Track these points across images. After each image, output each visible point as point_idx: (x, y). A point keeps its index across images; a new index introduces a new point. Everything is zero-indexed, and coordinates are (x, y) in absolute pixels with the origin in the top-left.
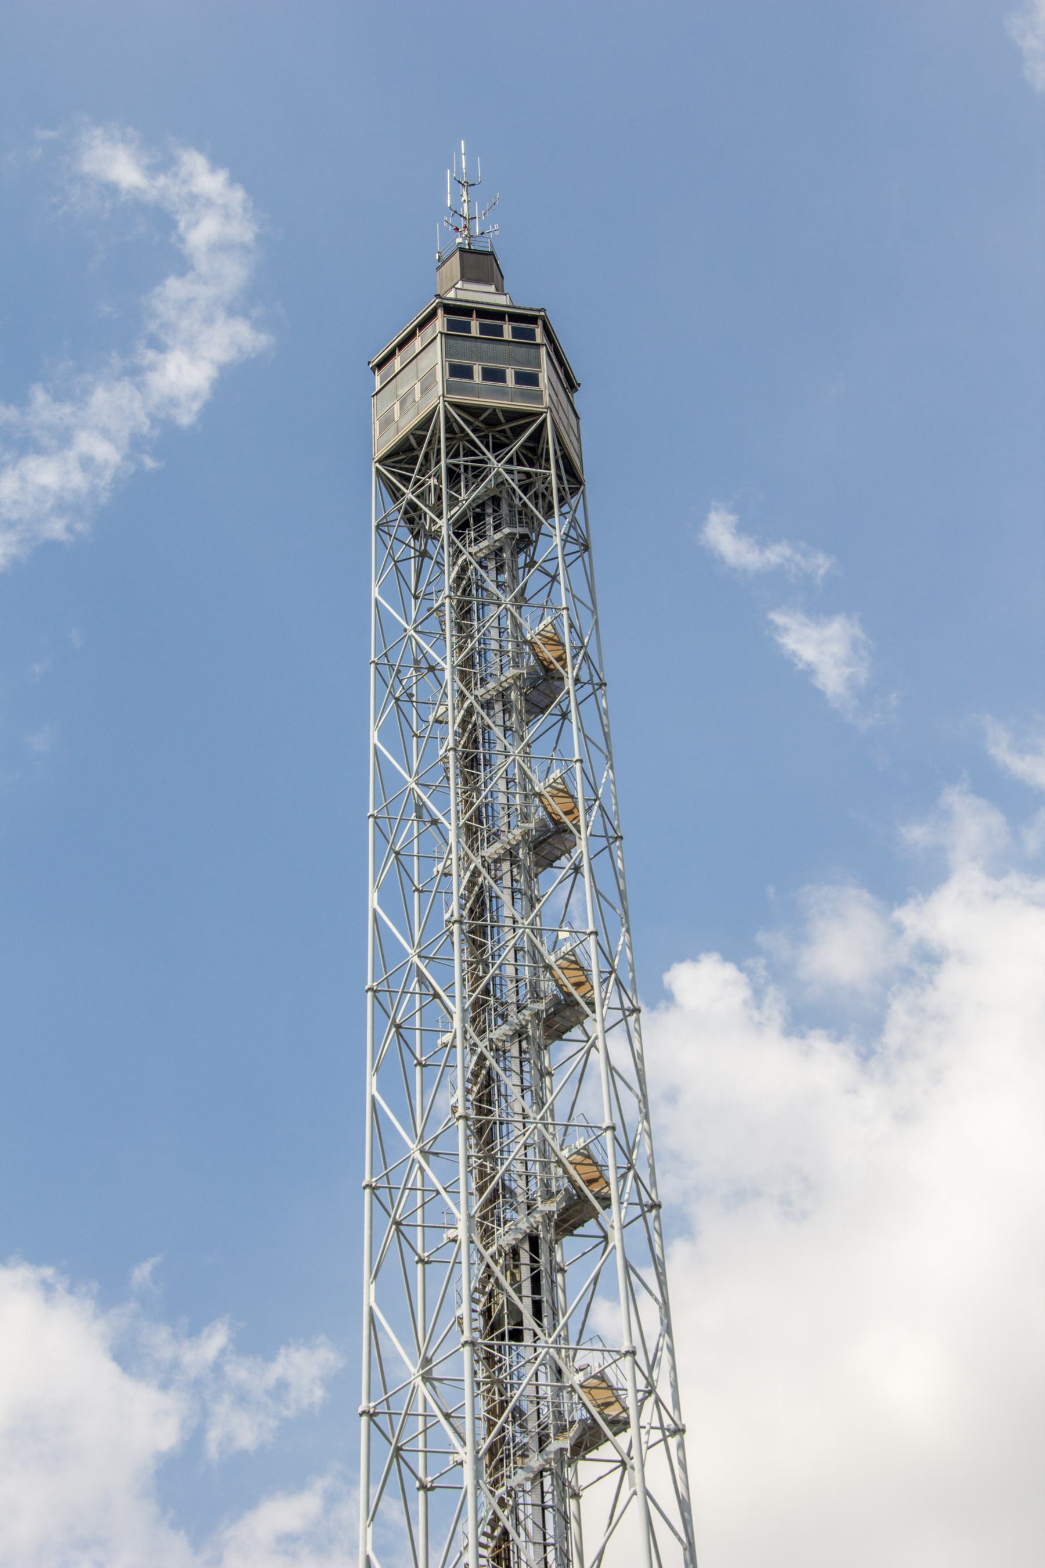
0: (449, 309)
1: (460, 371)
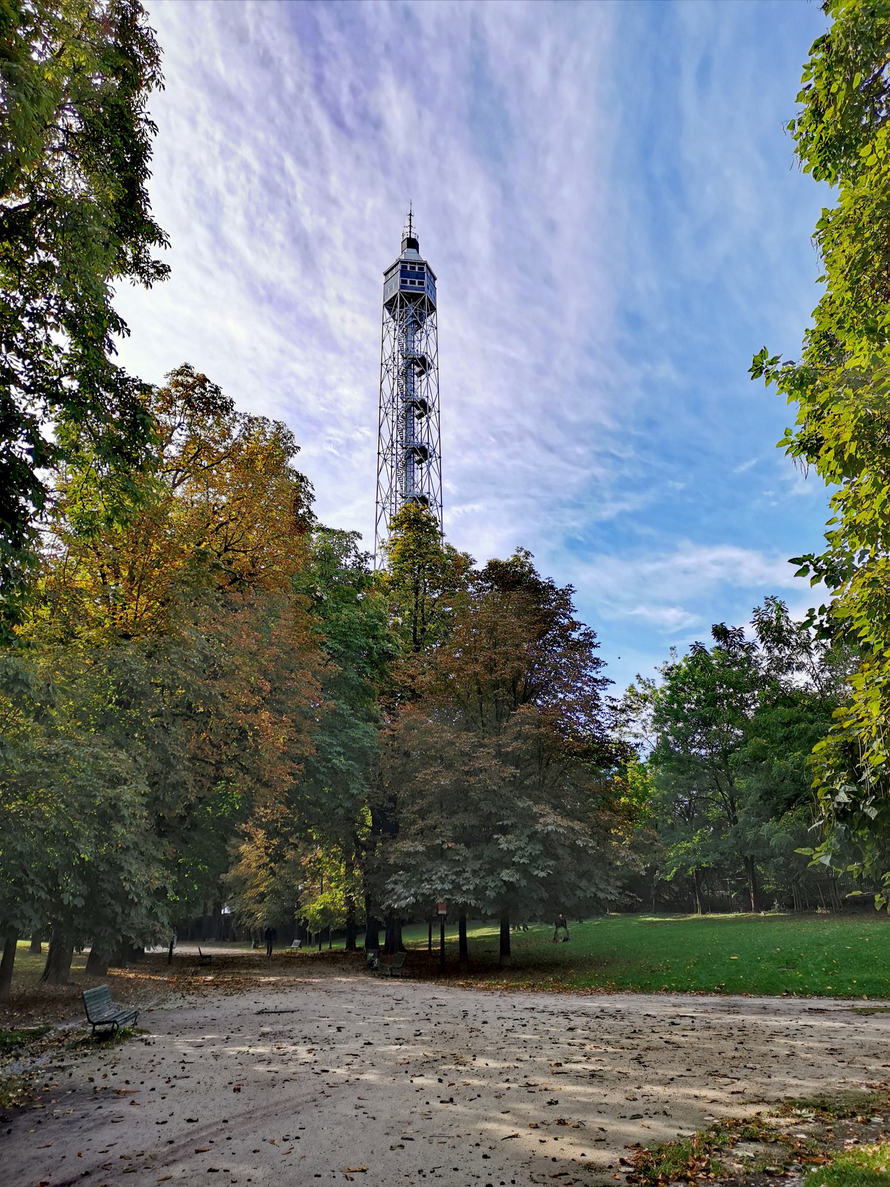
0: (402, 262)
1: (404, 282)
